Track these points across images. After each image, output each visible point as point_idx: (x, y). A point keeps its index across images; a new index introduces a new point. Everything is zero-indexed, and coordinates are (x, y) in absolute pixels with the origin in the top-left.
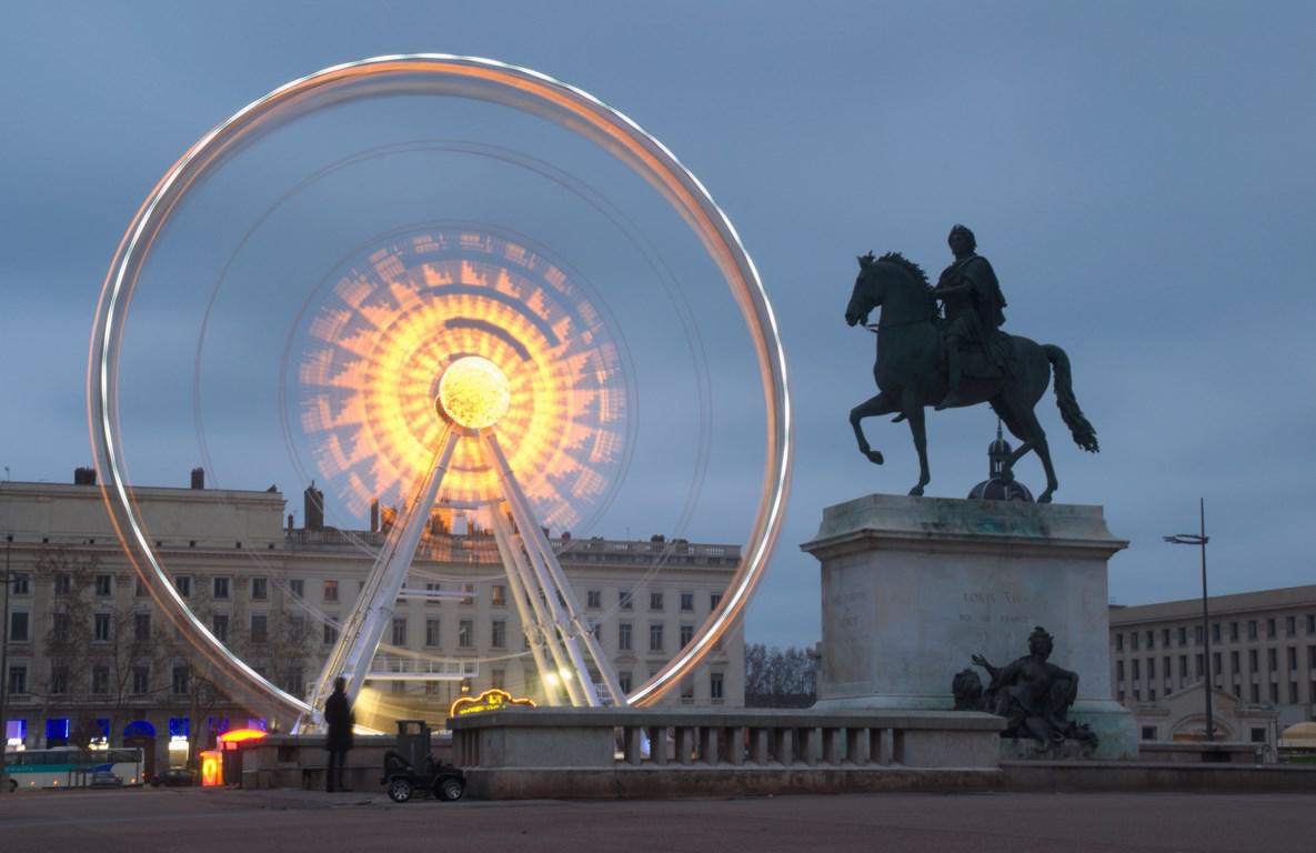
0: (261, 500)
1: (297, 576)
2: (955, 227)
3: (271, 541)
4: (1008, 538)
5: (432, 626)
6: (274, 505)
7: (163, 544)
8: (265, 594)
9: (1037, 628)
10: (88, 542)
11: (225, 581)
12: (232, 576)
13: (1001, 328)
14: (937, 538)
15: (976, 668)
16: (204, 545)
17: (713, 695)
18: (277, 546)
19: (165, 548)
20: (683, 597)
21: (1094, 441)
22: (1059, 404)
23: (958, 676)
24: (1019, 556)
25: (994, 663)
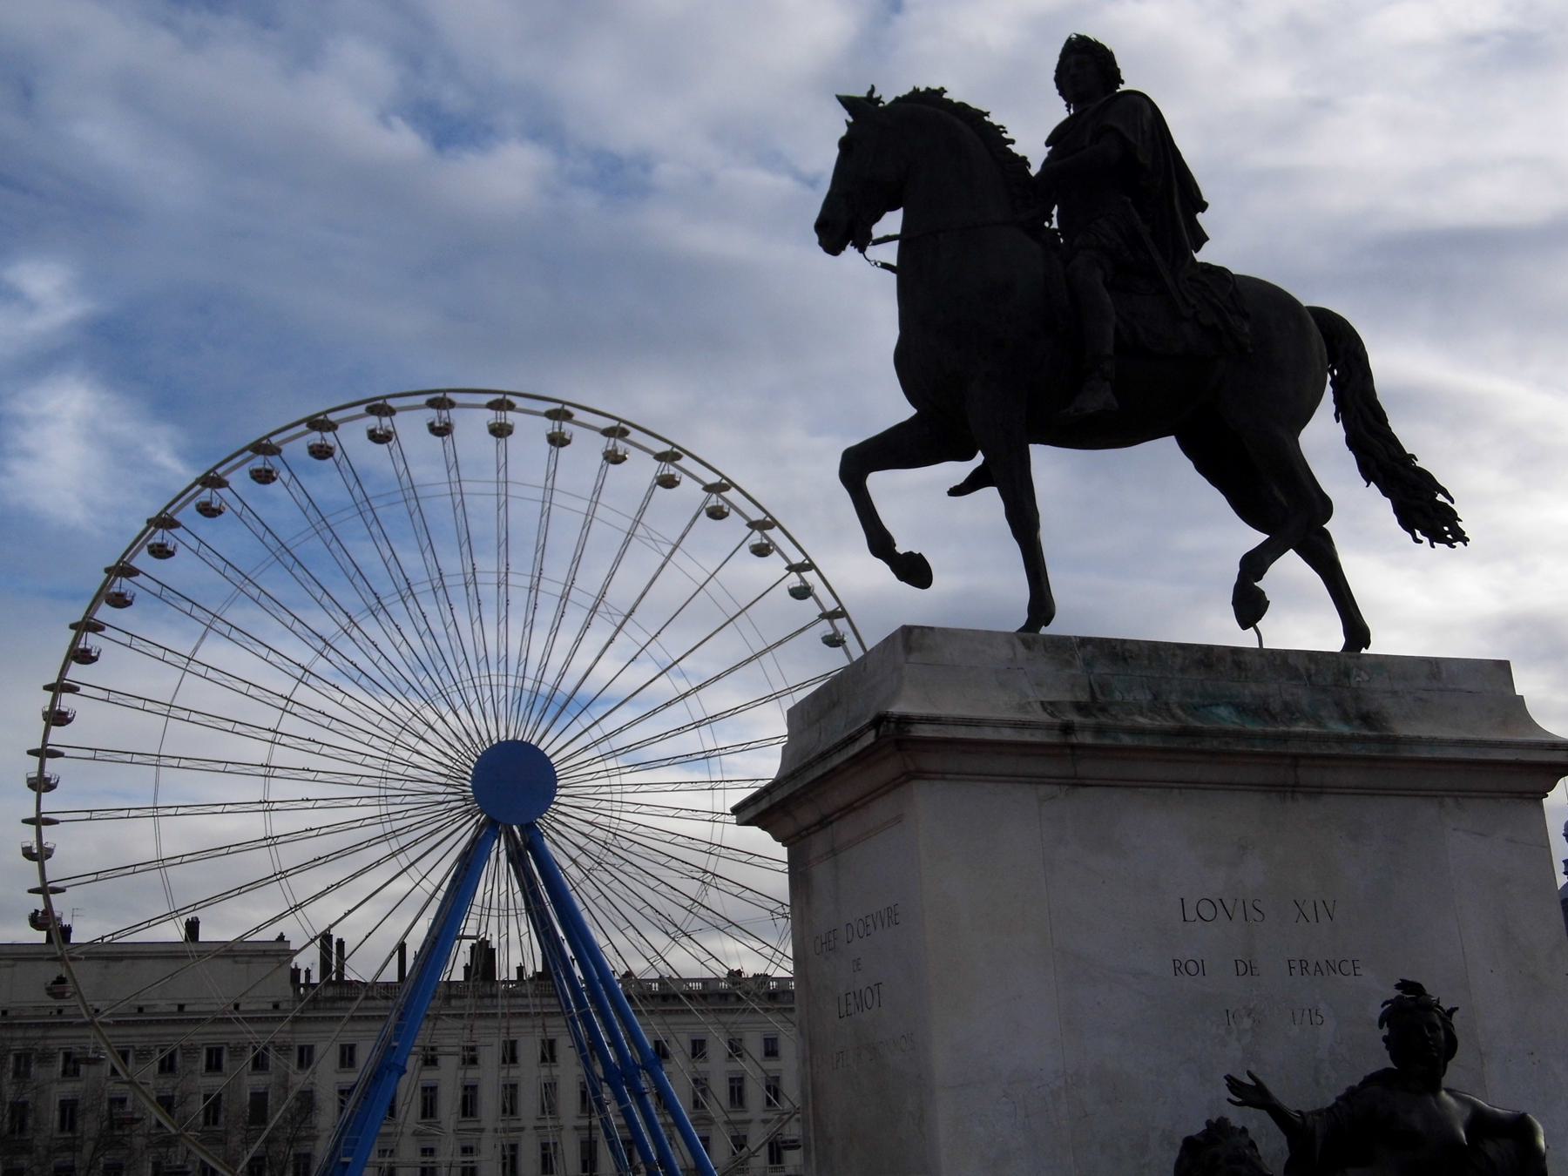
0: (264, 951)
1: (303, 1039)
2: (1070, 40)
3: (275, 999)
4: (1285, 738)
5: (736, 1085)
6: (279, 955)
7: (145, 1010)
8: (268, 1065)
9: (1404, 985)
10: (55, 1013)
11: (219, 1051)
12: (227, 1044)
13: (1201, 256)
14: (1088, 739)
15: (1238, 1117)
16: (196, 1008)
17: (772, 1161)
18: (283, 1006)
19: (66, 1017)
20: (766, 1041)
21: (1450, 517)
22: (1353, 442)
23: (1189, 1143)
24: (1317, 791)
25: (1291, 1101)
